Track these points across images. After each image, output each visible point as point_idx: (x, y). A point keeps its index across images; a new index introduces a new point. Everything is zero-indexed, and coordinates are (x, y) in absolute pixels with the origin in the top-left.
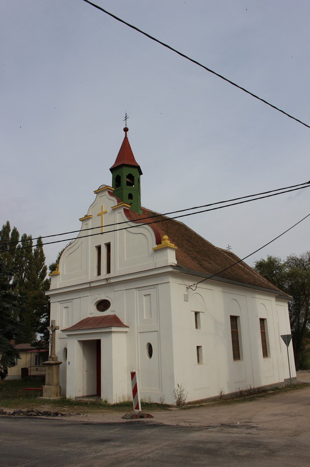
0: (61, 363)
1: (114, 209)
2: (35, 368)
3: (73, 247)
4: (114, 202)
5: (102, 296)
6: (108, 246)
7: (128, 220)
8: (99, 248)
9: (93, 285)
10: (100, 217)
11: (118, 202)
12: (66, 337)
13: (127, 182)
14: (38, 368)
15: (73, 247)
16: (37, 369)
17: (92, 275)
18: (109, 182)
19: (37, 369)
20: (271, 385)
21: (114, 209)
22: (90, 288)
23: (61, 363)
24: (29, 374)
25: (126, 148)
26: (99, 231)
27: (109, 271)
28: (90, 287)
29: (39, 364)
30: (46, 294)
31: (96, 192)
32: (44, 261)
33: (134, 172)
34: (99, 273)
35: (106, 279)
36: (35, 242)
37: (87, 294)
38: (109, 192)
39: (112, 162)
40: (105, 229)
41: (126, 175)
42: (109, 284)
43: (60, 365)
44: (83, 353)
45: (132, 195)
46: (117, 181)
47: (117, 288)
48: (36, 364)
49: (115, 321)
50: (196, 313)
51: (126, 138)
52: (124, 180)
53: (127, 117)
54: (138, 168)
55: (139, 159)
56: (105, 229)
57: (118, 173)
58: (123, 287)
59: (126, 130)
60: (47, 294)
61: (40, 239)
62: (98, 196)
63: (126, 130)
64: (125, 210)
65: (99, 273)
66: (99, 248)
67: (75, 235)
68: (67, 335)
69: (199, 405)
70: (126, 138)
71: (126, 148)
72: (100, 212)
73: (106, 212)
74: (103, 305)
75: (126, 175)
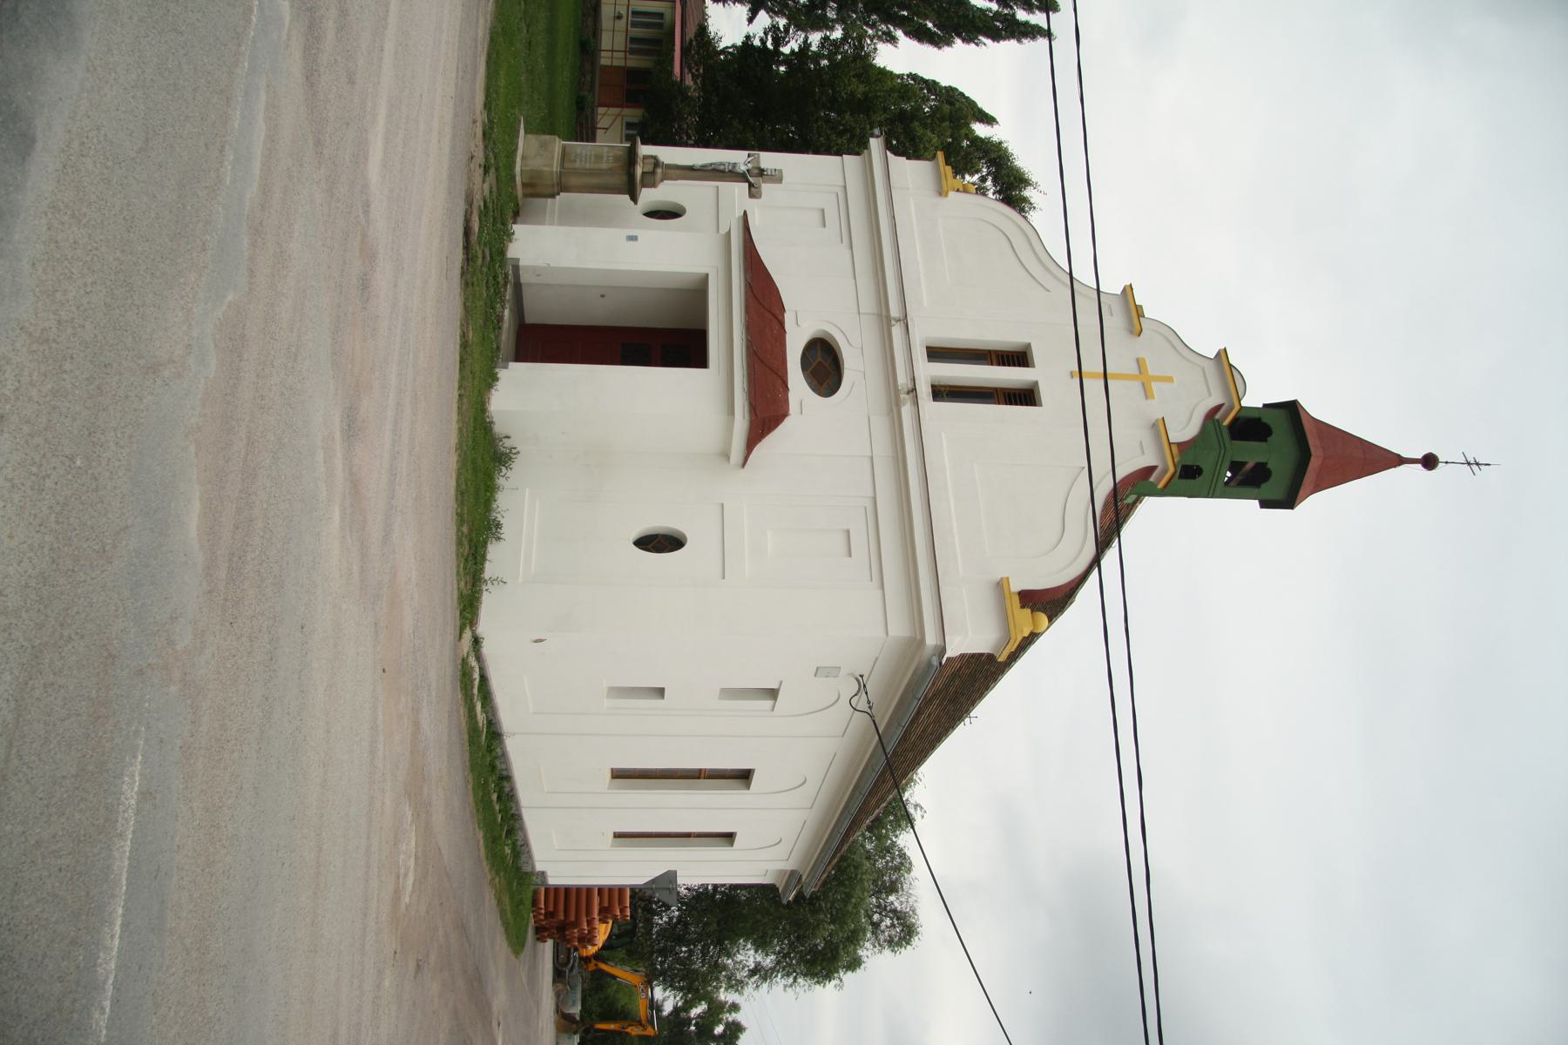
0: (634, 199)
1: (1158, 428)
2: (624, 13)
3: (1041, 262)
4: (1185, 428)
5: (857, 363)
6: (1026, 396)
7: (1118, 479)
8: (1020, 358)
9: (897, 331)
10: (1134, 370)
11: (1179, 445)
12: (723, 231)
13: (1244, 464)
14: (624, 21)
15: (1041, 262)
16: (619, 17)
17: (931, 327)
18: (1255, 398)
19: (619, 17)
20: (526, 844)
21: (1158, 428)
22: (885, 321)
23: (634, 199)
24: (601, 110)
25: (1364, 459)
26: (1092, 364)
27: (942, 393)
28: (888, 317)
29: (634, 25)
30: (873, 141)
31: (1222, 355)
32: (967, 40)
33: (1271, 489)
34: (937, 354)
35: (914, 389)
36: (1038, 18)
37: (868, 303)
38: (1219, 407)
39: (1319, 408)
40: (1094, 387)
41: (1268, 454)
42: (897, 396)
43: (627, 197)
44: (666, 290)
45: (1194, 478)
46: (1250, 426)
47: (881, 426)
48: (635, 13)
49: (766, 413)
50: (773, 694)
51: (1399, 460)
52: (1251, 453)
53: (1475, 467)
54: (1289, 502)
55: (1318, 505)
56: (1094, 387)
57: (1279, 424)
58: (882, 448)
59: (1429, 462)
60: (875, 144)
61: (1048, 34)
62: (1207, 364)
63: (1429, 462)
64: (1149, 470)
65: (937, 354)
66: (1020, 358)
67: (1084, 275)
68: (729, 233)
69: (472, 681)
70: (1399, 460)
71: (1364, 459)
72: (1152, 370)
73: (1147, 394)
74: (825, 365)
75: (1268, 454)
